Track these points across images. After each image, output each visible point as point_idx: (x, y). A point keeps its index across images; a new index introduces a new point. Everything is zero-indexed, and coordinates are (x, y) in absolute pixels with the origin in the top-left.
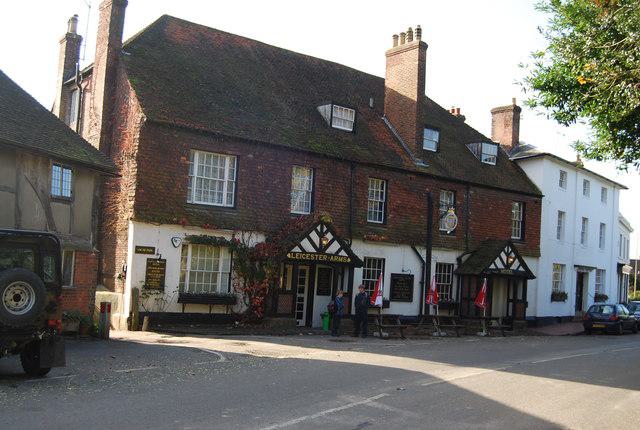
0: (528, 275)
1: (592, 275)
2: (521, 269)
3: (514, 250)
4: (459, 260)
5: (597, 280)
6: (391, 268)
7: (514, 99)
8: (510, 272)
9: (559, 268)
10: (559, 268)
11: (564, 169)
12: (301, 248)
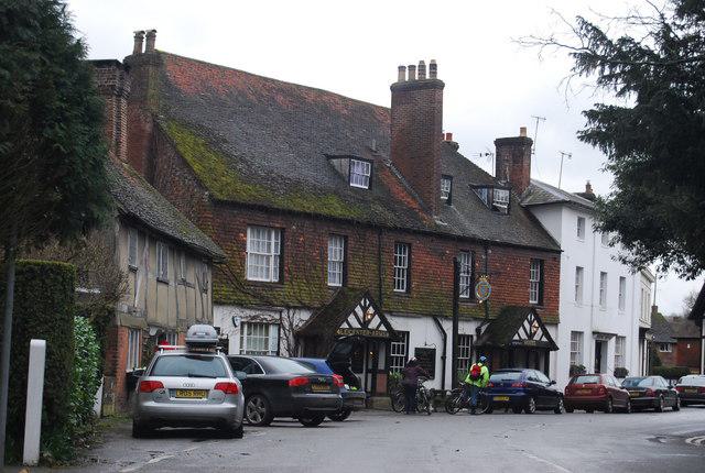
0: (552, 346)
1: (612, 343)
2: (544, 339)
3: (538, 319)
4: (478, 330)
5: (617, 349)
6: (416, 342)
7: (588, 186)
8: (532, 343)
9: (576, 335)
10: (576, 335)
11: (582, 216)
12: (349, 324)
